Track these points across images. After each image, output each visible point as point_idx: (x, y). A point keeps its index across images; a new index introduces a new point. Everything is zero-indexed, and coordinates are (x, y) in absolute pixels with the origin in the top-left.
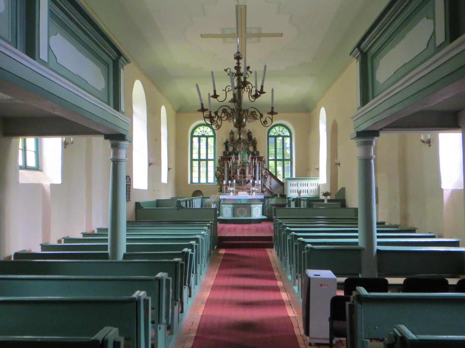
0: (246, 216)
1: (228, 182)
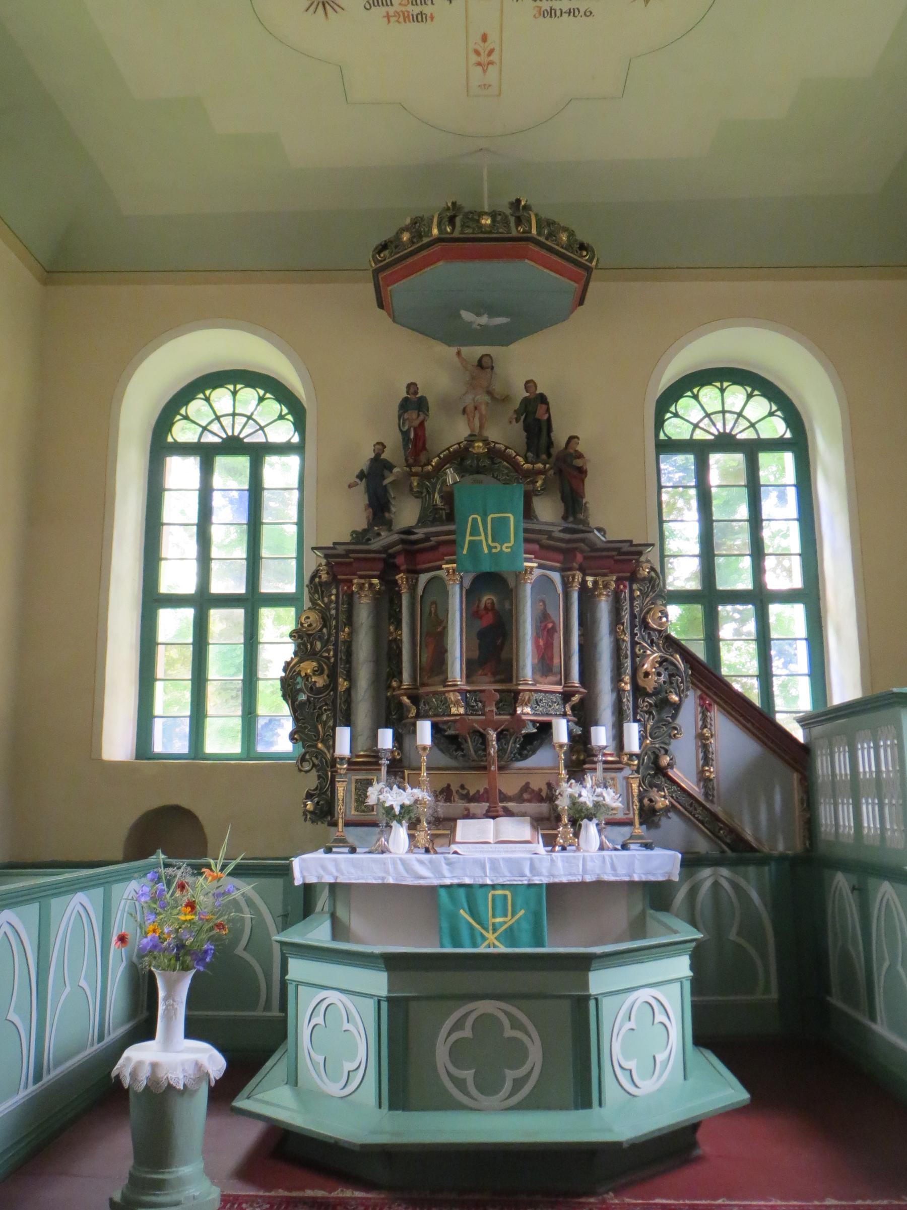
0: (535, 1102)
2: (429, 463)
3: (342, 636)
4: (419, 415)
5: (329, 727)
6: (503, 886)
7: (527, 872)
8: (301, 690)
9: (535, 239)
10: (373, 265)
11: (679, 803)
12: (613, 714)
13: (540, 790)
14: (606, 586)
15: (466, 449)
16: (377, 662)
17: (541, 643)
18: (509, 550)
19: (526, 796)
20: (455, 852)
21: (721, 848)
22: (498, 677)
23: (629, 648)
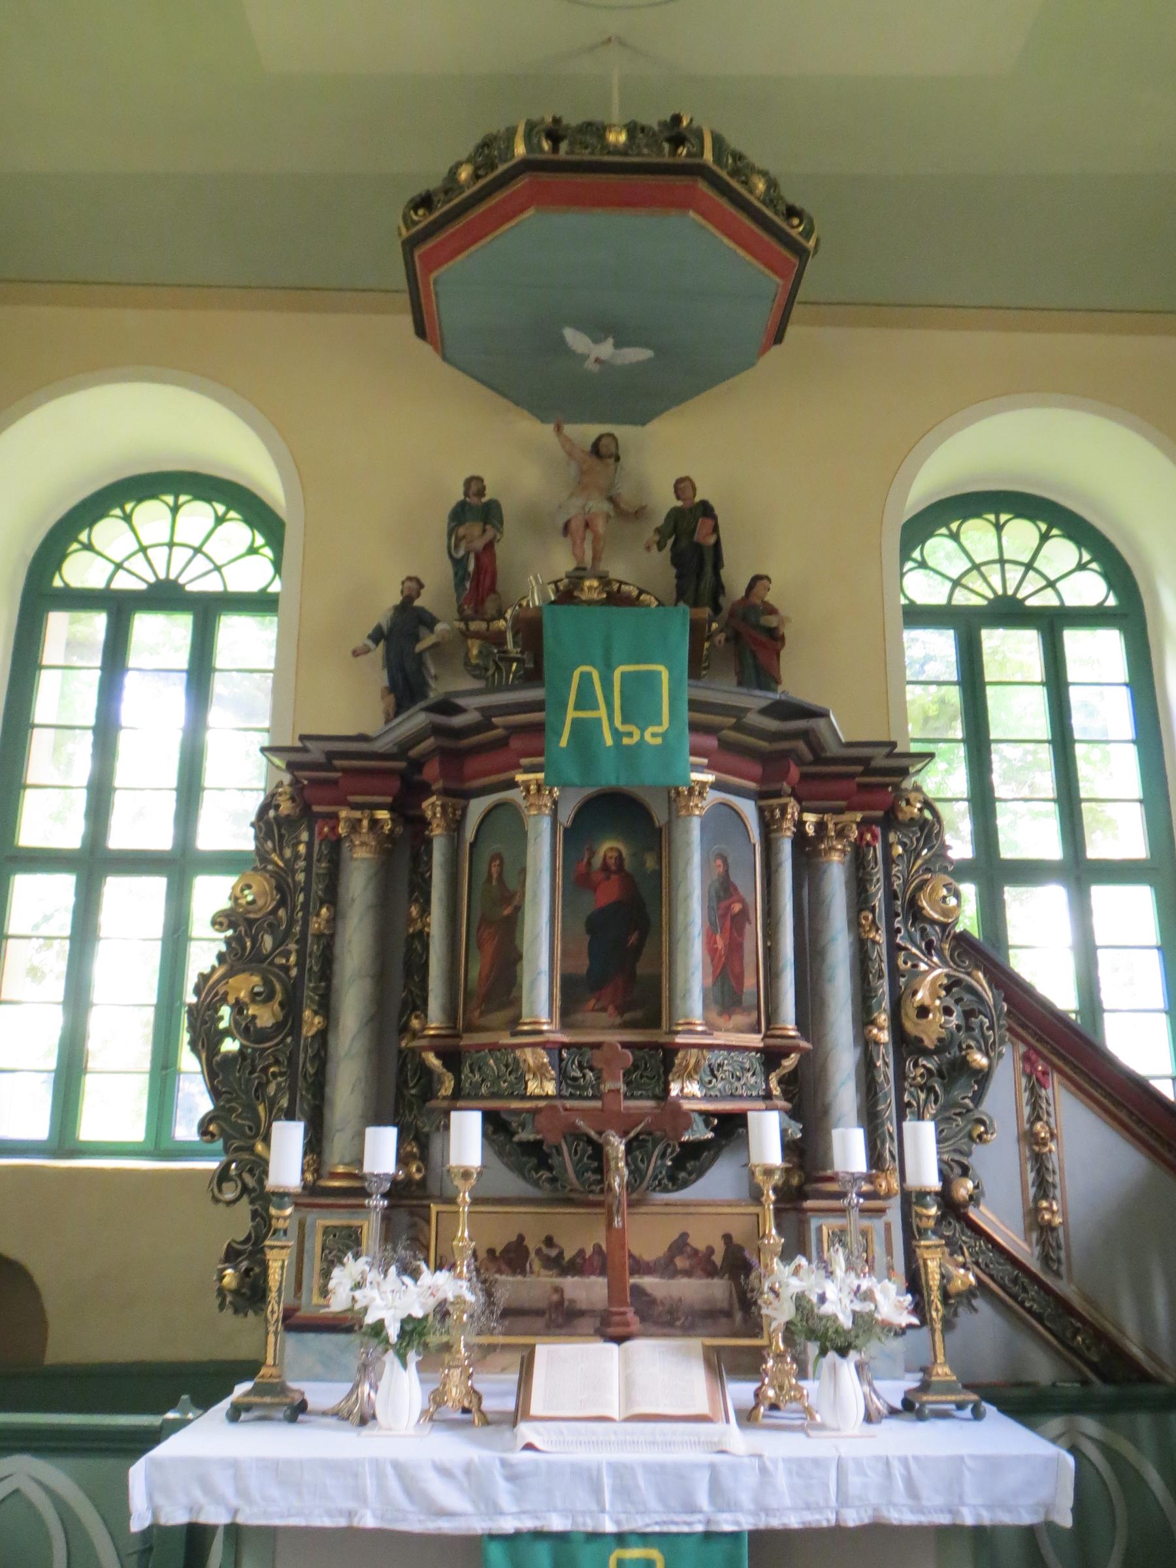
2: (501, 615)
3: (316, 925)
4: (484, 531)
6: (645, 1538)
7: (703, 1501)
8: (226, 1033)
9: (709, 168)
10: (404, 231)
11: (991, 1277)
13: (710, 1250)
14: (841, 834)
16: (381, 976)
17: (720, 944)
18: (659, 741)
19: (681, 1262)
20: (529, 1447)
21: (1080, 1372)
22: (628, 1016)
23: (885, 958)
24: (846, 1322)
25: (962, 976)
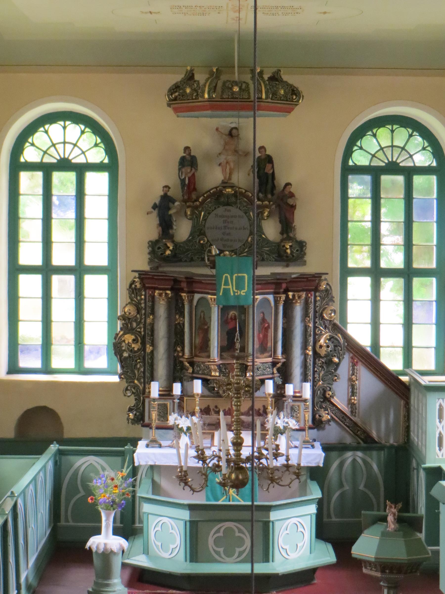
1: (170, 389)
2: (197, 200)
3: (149, 321)
4: (191, 170)
5: (141, 372)
11: (336, 416)
12: (301, 367)
13: (259, 410)
14: (299, 297)
15: (221, 191)
18: (244, 294)
23: (312, 330)
24: (282, 428)
25: (334, 335)
